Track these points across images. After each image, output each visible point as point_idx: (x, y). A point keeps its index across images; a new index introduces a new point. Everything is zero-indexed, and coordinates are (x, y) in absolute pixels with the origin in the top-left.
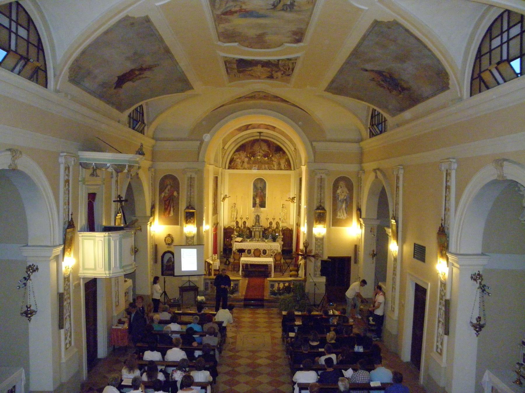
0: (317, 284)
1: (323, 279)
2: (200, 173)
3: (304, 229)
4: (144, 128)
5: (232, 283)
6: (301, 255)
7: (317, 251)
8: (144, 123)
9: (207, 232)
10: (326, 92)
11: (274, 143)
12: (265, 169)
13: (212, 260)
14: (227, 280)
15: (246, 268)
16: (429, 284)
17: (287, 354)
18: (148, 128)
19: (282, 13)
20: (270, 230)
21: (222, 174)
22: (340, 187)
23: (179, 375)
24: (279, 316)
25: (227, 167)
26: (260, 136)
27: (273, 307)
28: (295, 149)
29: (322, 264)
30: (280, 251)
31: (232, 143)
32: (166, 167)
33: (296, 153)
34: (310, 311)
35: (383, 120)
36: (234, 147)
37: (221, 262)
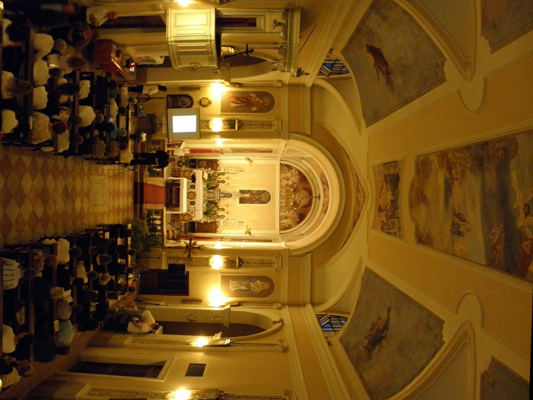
0: (160, 260)
2: (278, 135)
3: (218, 245)
4: (324, 75)
5: (160, 170)
6: (190, 243)
7: (194, 260)
8: (330, 75)
9: (214, 143)
11: (309, 212)
12: (281, 203)
13: (184, 148)
14: (164, 163)
17: (86, 230)
18: (323, 79)
19: (450, 224)
20: (216, 209)
22: (263, 283)
23: (65, 117)
24: (125, 219)
25: (282, 162)
26: (316, 197)
28: (303, 235)
29: (181, 265)
32: (283, 100)
33: (298, 236)
34: (131, 253)
35: (335, 329)
36: (304, 170)
37: (181, 157)
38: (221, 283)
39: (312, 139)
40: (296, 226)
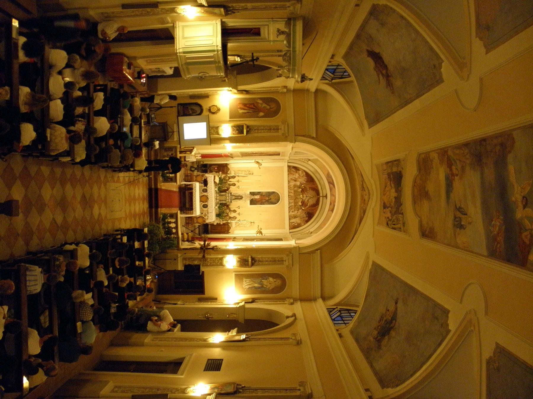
1: (180, 267)
2: (285, 138)
3: (231, 245)
4: (327, 79)
5: (173, 175)
6: (205, 244)
8: (332, 80)
9: (224, 148)
10: (494, 346)
11: (316, 211)
12: (289, 203)
13: (195, 154)
14: (176, 170)
15: (188, 188)
16: (182, 377)
18: (326, 84)
19: (451, 218)
21: (283, 159)
22: (275, 280)
23: (81, 128)
25: (290, 164)
26: (323, 197)
27: (150, 218)
28: (311, 233)
29: (196, 265)
30: (207, 222)
31: (312, 167)
32: (288, 104)
33: (307, 234)
35: (346, 322)
37: (193, 163)
38: (236, 281)
39: (318, 141)
40: (305, 224)
